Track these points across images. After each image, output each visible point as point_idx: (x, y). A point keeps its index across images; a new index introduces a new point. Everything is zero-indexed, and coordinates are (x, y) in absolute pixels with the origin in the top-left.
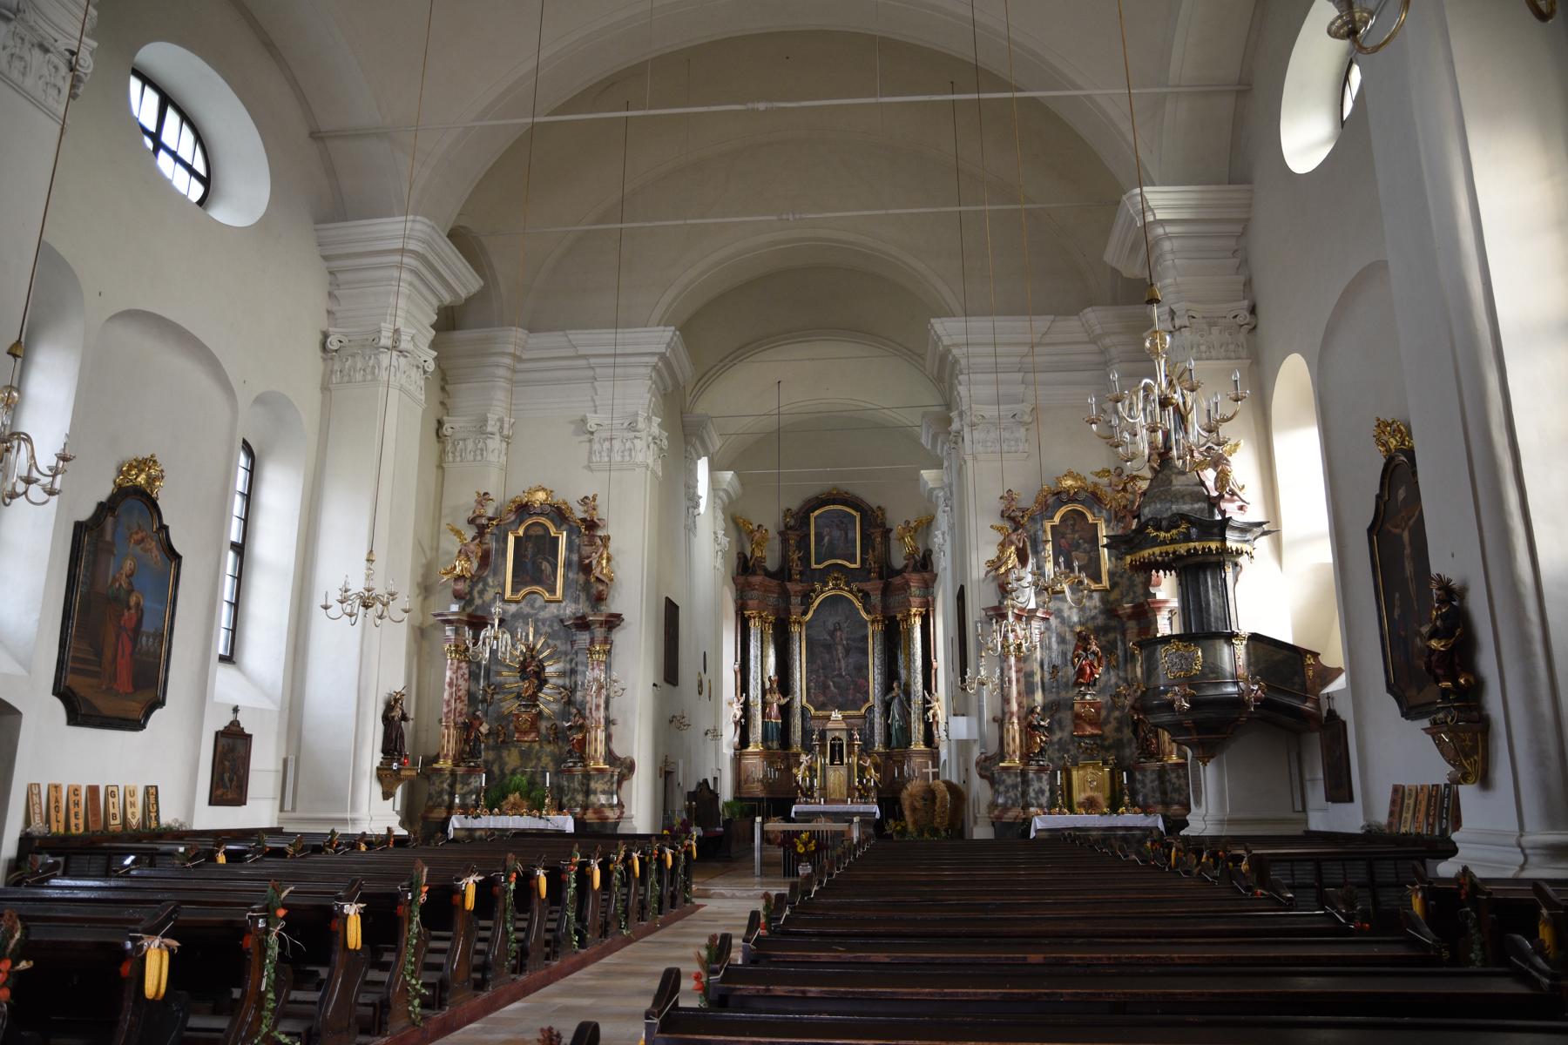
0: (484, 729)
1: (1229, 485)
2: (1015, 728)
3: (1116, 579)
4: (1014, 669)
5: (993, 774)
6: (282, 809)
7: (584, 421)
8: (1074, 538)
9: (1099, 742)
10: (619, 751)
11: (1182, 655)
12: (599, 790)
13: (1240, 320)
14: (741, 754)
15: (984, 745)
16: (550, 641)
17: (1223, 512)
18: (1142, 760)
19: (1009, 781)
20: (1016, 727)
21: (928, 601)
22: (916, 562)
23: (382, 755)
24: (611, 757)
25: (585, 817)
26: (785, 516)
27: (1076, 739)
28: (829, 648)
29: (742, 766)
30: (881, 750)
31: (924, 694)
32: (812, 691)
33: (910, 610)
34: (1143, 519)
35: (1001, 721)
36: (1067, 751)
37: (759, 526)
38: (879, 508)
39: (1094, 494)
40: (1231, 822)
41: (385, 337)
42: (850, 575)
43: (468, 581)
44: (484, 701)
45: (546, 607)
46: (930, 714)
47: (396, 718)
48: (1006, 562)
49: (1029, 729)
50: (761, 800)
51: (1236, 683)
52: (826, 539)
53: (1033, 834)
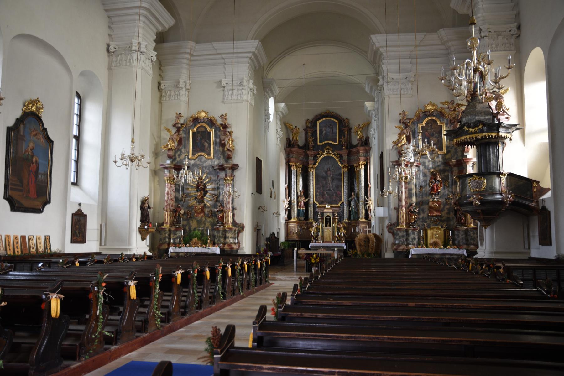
0: (182, 212)
1: (502, 108)
2: (404, 212)
3: (449, 149)
4: (404, 187)
5: (394, 231)
6: (100, 245)
7: (220, 82)
8: (431, 132)
9: (439, 218)
10: (238, 221)
11: (477, 182)
12: (230, 237)
13: (512, 32)
14: (288, 222)
15: (390, 219)
16: (208, 175)
17: (499, 120)
18: (458, 226)
19: (401, 234)
20: (404, 212)
21: (367, 159)
22: (362, 142)
23: (140, 223)
24: (234, 223)
25: (224, 248)
26: (307, 122)
27: (430, 217)
28: (325, 178)
29: (289, 227)
30: (347, 221)
31: (365, 198)
32: (318, 196)
33: (359, 163)
34: (462, 123)
35: (398, 209)
36: (426, 222)
37: (296, 127)
38: (347, 119)
39: (441, 112)
40: (496, 253)
41: (134, 46)
42: (334, 148)
43: (173, 151)
44: (182, 200)
45: (206, 161)
46: (367, 206)
47: (146, 208)
48: (401, 142)
49: (410, 213)
50: (297, 241)
51: (501, 194)
52: (324, 132)
53: (410, 256)
